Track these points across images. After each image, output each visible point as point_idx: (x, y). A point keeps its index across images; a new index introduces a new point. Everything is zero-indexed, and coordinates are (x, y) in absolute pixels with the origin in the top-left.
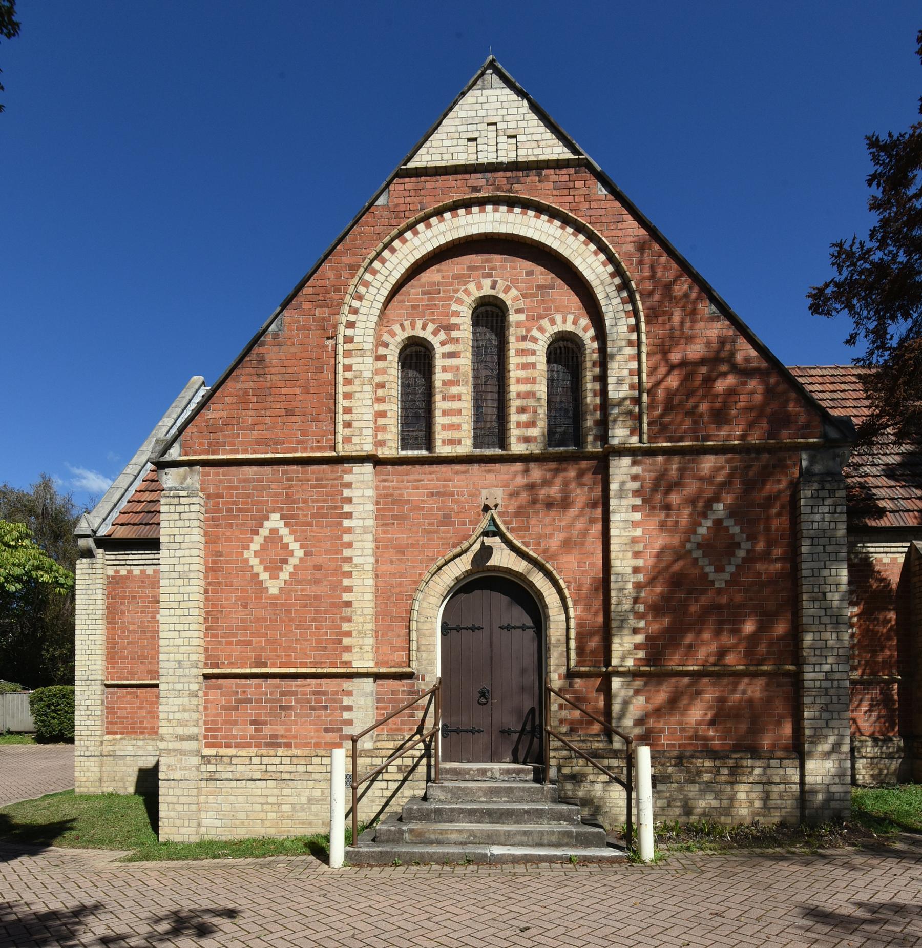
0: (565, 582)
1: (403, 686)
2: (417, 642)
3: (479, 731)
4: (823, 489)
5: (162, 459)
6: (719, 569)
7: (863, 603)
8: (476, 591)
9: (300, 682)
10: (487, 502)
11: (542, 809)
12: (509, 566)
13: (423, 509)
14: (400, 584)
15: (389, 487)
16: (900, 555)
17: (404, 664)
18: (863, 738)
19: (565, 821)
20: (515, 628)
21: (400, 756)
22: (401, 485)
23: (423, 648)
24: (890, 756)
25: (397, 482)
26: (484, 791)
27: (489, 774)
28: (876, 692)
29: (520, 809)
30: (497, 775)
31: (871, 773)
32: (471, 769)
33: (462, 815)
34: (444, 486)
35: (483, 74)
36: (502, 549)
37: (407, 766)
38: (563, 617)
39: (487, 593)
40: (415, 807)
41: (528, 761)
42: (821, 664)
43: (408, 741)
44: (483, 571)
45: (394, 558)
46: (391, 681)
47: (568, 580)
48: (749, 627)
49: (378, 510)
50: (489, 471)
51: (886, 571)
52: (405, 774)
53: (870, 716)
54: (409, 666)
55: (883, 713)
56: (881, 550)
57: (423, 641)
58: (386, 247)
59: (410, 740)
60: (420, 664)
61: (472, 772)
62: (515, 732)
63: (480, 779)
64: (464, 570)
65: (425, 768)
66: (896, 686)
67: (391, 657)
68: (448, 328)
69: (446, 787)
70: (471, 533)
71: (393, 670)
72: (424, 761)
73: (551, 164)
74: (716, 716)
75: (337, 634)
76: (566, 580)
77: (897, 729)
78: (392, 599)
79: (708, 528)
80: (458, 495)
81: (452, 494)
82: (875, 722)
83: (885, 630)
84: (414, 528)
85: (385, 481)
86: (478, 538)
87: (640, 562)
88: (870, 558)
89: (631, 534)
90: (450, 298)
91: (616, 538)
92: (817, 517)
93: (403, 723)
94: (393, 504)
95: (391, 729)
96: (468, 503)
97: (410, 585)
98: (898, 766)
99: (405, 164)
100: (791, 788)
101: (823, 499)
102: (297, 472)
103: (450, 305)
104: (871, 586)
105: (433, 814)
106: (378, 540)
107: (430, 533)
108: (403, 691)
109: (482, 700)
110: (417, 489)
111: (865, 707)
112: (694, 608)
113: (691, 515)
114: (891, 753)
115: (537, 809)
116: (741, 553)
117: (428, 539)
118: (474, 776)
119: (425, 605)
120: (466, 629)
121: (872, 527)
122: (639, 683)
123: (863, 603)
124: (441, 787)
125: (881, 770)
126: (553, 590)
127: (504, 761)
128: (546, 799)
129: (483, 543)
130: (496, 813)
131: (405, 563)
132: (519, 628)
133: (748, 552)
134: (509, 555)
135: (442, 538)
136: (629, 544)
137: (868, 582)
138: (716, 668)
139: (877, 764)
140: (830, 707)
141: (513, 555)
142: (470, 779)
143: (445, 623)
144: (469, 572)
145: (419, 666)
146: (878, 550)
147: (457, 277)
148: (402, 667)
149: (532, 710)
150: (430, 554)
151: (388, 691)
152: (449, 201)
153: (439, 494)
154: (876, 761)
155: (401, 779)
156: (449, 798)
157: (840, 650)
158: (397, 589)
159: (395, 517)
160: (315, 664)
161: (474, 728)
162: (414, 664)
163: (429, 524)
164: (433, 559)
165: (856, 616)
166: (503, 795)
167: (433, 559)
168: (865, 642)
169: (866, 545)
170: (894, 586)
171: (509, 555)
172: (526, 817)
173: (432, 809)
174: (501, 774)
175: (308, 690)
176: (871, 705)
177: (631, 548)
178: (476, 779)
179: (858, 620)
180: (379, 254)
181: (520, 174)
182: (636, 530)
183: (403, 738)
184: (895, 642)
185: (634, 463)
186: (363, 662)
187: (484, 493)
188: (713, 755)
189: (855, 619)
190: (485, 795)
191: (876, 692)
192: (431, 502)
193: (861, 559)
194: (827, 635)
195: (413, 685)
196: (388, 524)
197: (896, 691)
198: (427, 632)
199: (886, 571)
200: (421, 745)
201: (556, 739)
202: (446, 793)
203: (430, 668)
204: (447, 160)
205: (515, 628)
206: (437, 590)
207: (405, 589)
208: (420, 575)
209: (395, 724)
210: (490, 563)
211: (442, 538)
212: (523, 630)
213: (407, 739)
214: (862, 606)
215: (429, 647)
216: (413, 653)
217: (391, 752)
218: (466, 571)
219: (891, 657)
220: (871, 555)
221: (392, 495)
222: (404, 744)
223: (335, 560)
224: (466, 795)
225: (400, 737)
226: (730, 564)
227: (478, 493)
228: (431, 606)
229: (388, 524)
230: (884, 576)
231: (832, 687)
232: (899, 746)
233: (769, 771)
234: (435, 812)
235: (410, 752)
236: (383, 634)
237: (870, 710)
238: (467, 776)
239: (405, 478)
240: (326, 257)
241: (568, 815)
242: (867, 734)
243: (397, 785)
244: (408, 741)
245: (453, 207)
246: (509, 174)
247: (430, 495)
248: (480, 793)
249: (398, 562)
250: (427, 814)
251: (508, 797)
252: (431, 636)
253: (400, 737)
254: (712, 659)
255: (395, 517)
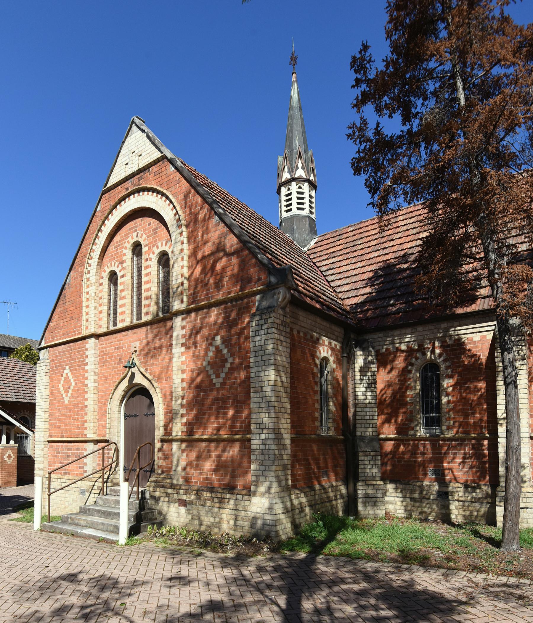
4: (261, 319)
5: (40, 347)
6: (218, 376)
7: (457, 376)
9: (73, 444)
16: (489, 332)
18: (457, 485)
23: (112, 427)
24: (479, 501)
28: (468, 449)
31: (463, 513)
35: (131, 128)
42: (260, 434)
48: (231, 413)
50: (134, 333)
51: (476, 347)
53: (463, 467)
55: (476, 464)
56: (471, 331)
58: (174, 207)
66: (486, 442)
68: (122, 262)
73: (152, 164)
74: (217, 466)
75: (82, 421)
77: (487, 478)
79: (213, 351)
82: (467, 472)
83: (476, 398)
85: (101, 344)
87: (184, 376)
88: (462, 339)
90: (122, 248)
92: (258, 338)
98: (487, 509)
99: (105, 186)
100: (248, 514)
101: (262, 325)
102: (81, 344)
103: (122, 251)
104: (463, 362)
111: (458, 460)
112: (208, 401)
113: (206, 344)
114: (479, 498)
116: (228, 365)
121: (459, 315)
122: (184, 445)
123: (457, 376)
125: (471, 512)
133: (231, 363)
137: (461, 358)
138: (215, 437)
139: (468, 506)
140: (265, 463)
146: (468, 331)
147: (125, 235)
152: (117, 200)
154: (467, 504)
157: (270, 424)
160: (77, 436)
165: (451, 386)
168: (459, 407)
169: (457, 328)
170: (484, 361)
175: (75, 448)
176: (464, 458)
179: (453, 389)
180: (97, 235)
181: (143, 174)
184: (485, 407)
185: (183, 319)
186: (91, 435)
188: (211, 490)
189: (451, 389)
191: (468, 449)
193: (455, 340)
194: (262, 415)
197: (487, 446)
199: (476, 347)
204: (123, 176)
214: (455, 378)
219: (481, 420)
220: (463, 336)
223: (82, 386)
226: (222, 372)
230: (475, 353)
231: (265, 449)
232: (487, 493)
233: (237, 503)
237: (463, 462)
239: (108, 342)
240: (82, 242)
242: (462, 482)
245: (119, 202)
246: (139, 176)
248: (112, 503)
254: (215, 432)
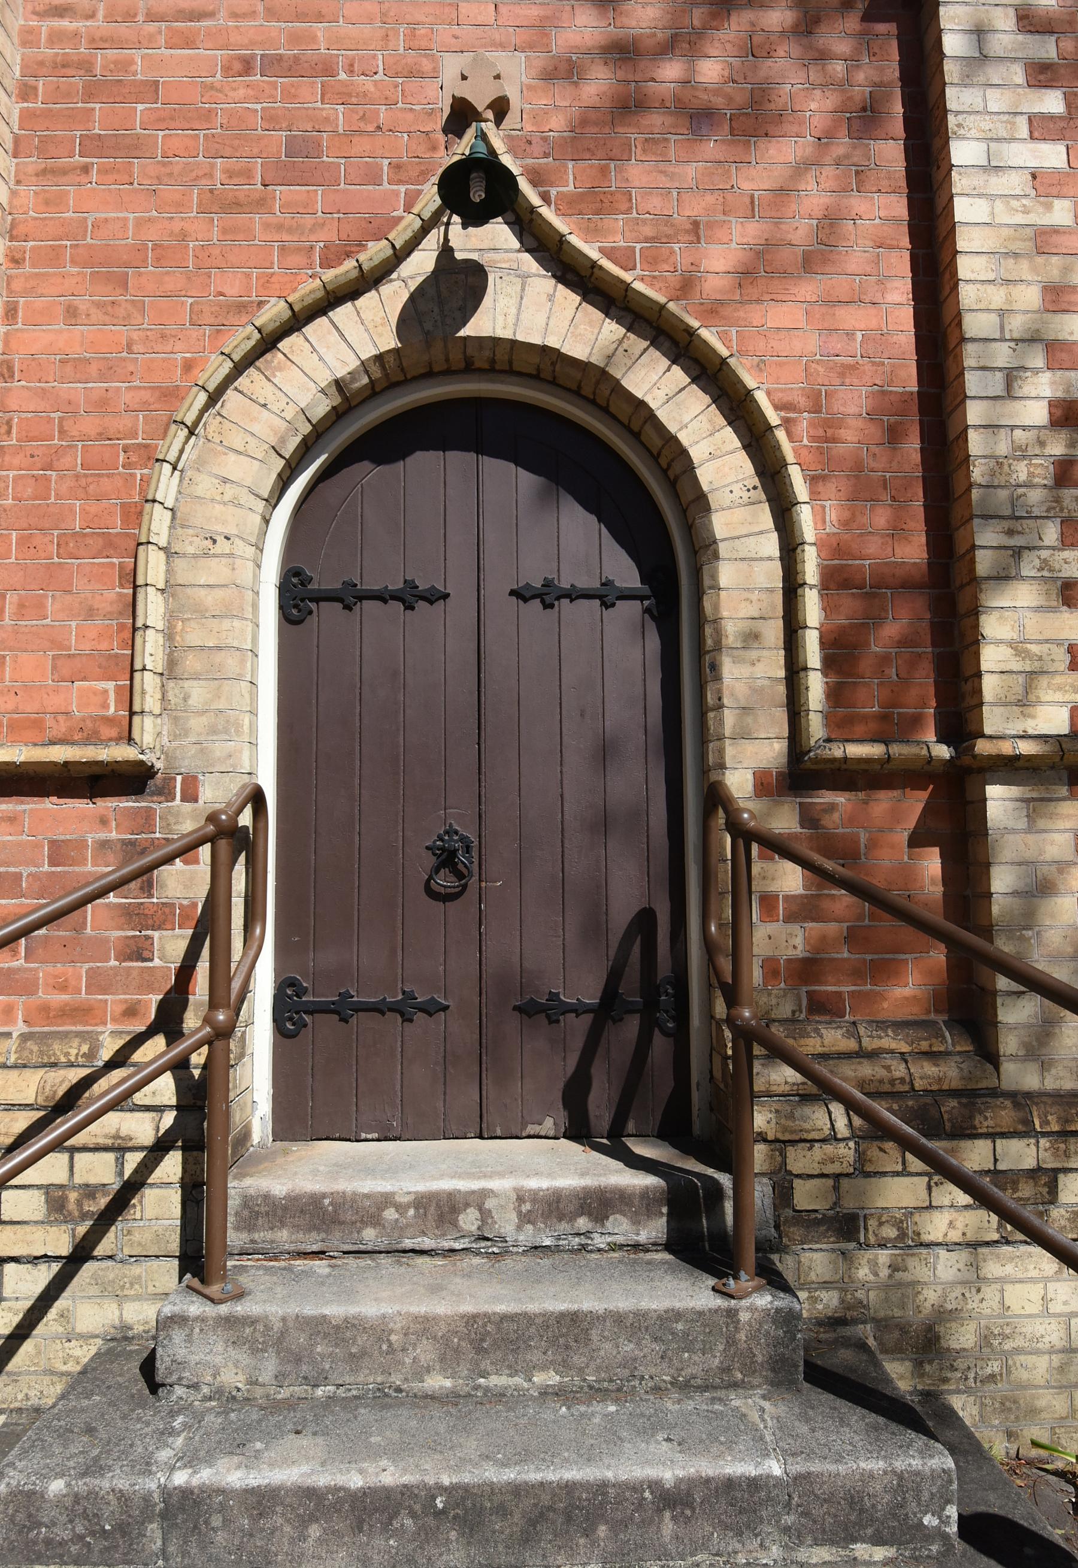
0: (777, 408)
1: (104, 822)
2: (169, 635)
3: (431, 1009)
8: (419, 455)
10: (466, 91)
11: (753, 1484)
12: (553, 342)
13: (208, 115)
14: (102, 404)
15: (76, 34)
17: (107, 732)
19: (878, 1540)
20: (574, 595)
21: (56, 1146)
22: (123, 30)
23: (191, 662)
25: (110, 19)
26: (446, 1341)
27: (469, 1221)
29: (635, 1487)
30: (506, 1224)
32: (387, 1200)
33: (314, 1531)
34: (294, 38)
36: (525, 277)
37: (90, 1191)
38: (771, 545)
39: (459, 460)
40: (57, 1486)
41: (631, 1127)
43: (113, 1064)
44: (449, 373)
45: (82, 303)
46: (49, 804)
47: (787, 398)
49: (26, 116)
52: (82, 1229)
54: (130, 740)
57: (193, 635)
59: (118, 1061)
60: (179, 730)
61: (390, 1214)
62: (577, 1010)
63: (427, 1243)
64: (368, 352)
65: (175, 1197)
67: (54, 702)
69: (251, 1321)
70: (400, 212)
71: (59, 754)
72: (172, 1165)
76: (777, 396)
78: (66, 461)
80: (351, 71)
81: (328, 70)
84: (170, 192)
86: (425, 230)
89: (1032, 219)
91: (976, 233)
93: (99, 983)
94: (89, 95)
95: (45, 1011)
96: (391, 103)
97: (145, 407)
105: (153, 1529)
106: (21, 229)
107: (235, 206)
108: (104, 845)
109: (444, 881)
110: (189, 43)
115: (730, 1484)
117: (224, 231)
118: (400, 1229)
119: (205, 485)
120: (382, 597)
124: (229, 1322)
126: (729, 438)
127: (531, 1129)
128: (749, 1368)
129: (446, 251)
130: (502, 1511)
131: (126, 321)
132: (587, 595)
134: (551, 298)
135: (280, 227)
136: (1028, 256)
141: (569, 298)
142: (383, 1243)
143: (297, 573)
144: (391, 360)
145: (174, 737)
148: (105, 742)
149: (645, 920)
150: (232, 286)
151: (38, 846)
153: (273, 65)
155: (65, 1250)
156: (267, 1375)
158: (89, 425)
159: (93, 145)
161: (409, 996)
162: (147, 730)
163: (230, 174)
164: (242, 308)
166: (535, 1356)
167: (242, 308)
171: (551, 298)
172: (668, 1527)
173: (147, 1498)
174: (526, 1219)
177: (1034, 270)
178: (408, 1243)
182: (1049, 207)
183: (91, 1055)
187: (451, 66)
190: (448, 1359)
192: (242, 92)
195: (147, 820)
196: (64, 172)
198: (210, 599)
200: (165, 1089)
201: (1021, 1237)
202: (254, 1351)
203: (219, 749)
205: (574, 595)
206: (255, 428)
207: (124, 422)
208: (188, 366)
209: (63, 988)
210: (478, 326)
211: (280, 227)
212: (607, 605)
213: (106, 1054)
215: (218, 657)
216: (149, 683)
217: (22, 1121)
218: (379, 358)
221: (86, 66)
222: (86, 1083)
224: (355, 1360)
225: (75, 1049)
227: (426, 65)
228: (230, 491)
229: (64, 172)
234: (165, 1516)
235: (113, 1121)
236: (21, 606)
238: (369, 1234)
241: (896, 1509)
243: (42, 1276)
244: (113, 1064)
247: (237, 66)
248: (425, 1352)
249: (97, 315)
250: (122, 1529)
251: (563, 1366)
252: (227, 613)
253: (75, 1049)
255: (93, 145)
